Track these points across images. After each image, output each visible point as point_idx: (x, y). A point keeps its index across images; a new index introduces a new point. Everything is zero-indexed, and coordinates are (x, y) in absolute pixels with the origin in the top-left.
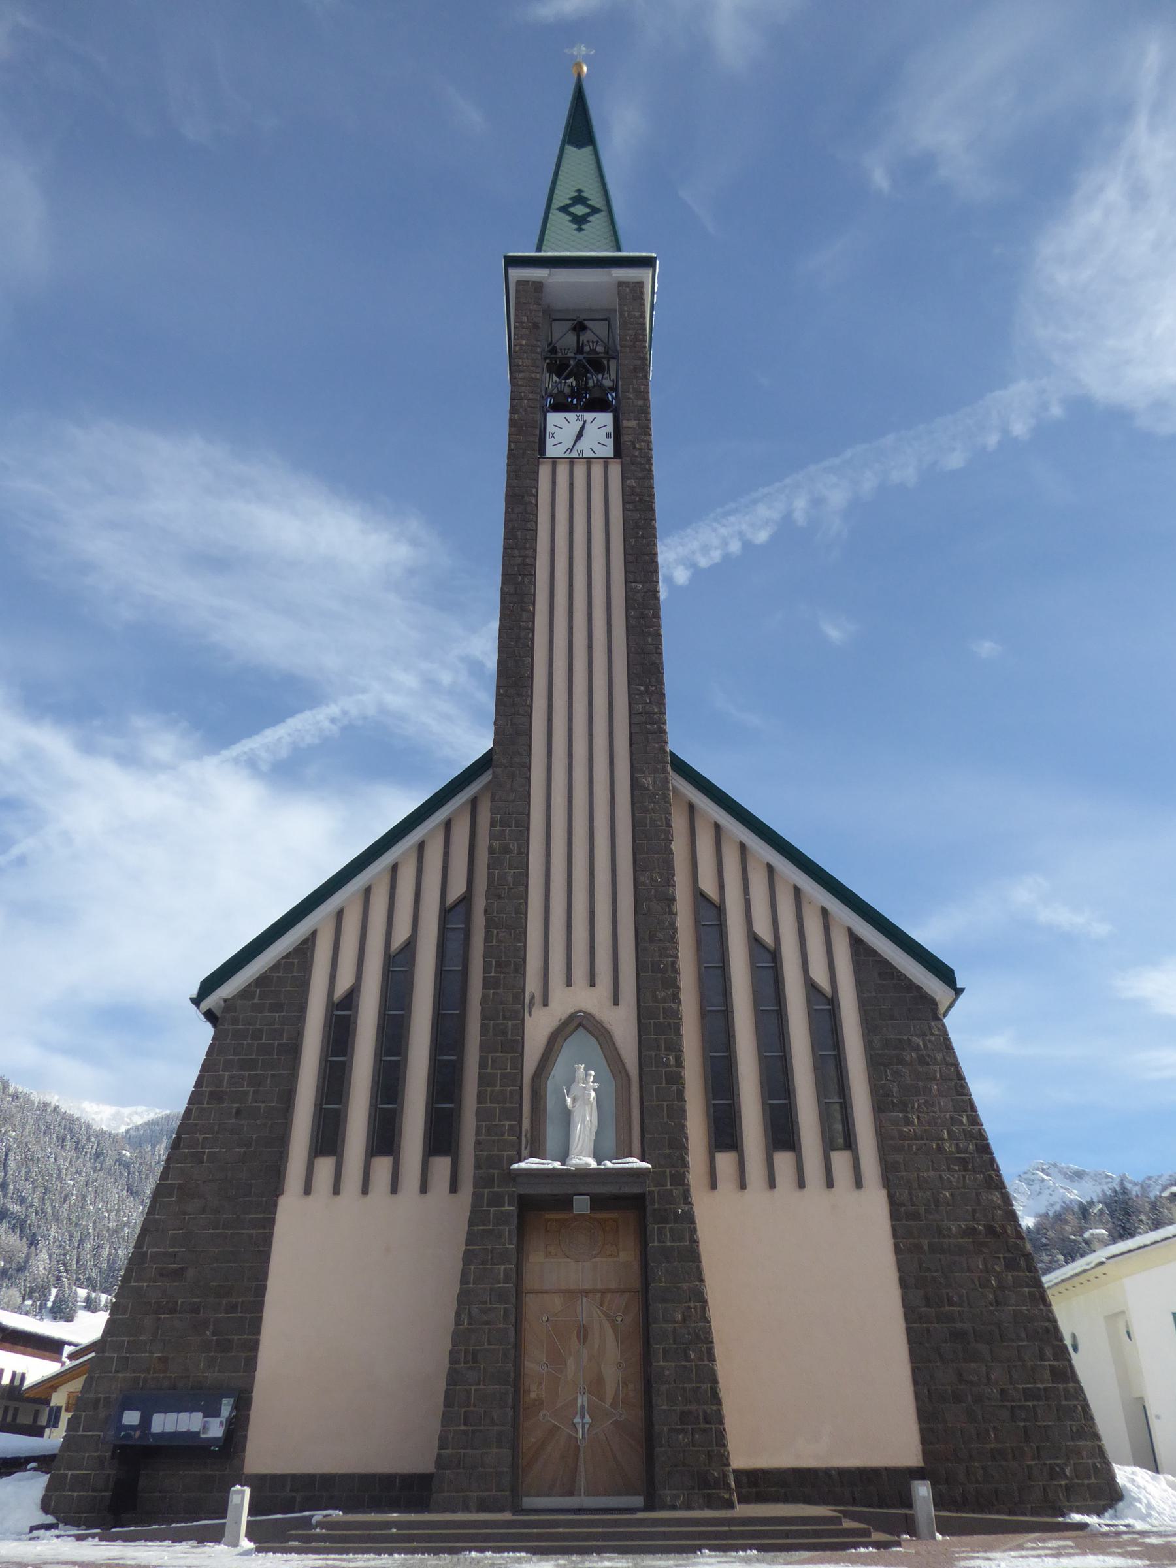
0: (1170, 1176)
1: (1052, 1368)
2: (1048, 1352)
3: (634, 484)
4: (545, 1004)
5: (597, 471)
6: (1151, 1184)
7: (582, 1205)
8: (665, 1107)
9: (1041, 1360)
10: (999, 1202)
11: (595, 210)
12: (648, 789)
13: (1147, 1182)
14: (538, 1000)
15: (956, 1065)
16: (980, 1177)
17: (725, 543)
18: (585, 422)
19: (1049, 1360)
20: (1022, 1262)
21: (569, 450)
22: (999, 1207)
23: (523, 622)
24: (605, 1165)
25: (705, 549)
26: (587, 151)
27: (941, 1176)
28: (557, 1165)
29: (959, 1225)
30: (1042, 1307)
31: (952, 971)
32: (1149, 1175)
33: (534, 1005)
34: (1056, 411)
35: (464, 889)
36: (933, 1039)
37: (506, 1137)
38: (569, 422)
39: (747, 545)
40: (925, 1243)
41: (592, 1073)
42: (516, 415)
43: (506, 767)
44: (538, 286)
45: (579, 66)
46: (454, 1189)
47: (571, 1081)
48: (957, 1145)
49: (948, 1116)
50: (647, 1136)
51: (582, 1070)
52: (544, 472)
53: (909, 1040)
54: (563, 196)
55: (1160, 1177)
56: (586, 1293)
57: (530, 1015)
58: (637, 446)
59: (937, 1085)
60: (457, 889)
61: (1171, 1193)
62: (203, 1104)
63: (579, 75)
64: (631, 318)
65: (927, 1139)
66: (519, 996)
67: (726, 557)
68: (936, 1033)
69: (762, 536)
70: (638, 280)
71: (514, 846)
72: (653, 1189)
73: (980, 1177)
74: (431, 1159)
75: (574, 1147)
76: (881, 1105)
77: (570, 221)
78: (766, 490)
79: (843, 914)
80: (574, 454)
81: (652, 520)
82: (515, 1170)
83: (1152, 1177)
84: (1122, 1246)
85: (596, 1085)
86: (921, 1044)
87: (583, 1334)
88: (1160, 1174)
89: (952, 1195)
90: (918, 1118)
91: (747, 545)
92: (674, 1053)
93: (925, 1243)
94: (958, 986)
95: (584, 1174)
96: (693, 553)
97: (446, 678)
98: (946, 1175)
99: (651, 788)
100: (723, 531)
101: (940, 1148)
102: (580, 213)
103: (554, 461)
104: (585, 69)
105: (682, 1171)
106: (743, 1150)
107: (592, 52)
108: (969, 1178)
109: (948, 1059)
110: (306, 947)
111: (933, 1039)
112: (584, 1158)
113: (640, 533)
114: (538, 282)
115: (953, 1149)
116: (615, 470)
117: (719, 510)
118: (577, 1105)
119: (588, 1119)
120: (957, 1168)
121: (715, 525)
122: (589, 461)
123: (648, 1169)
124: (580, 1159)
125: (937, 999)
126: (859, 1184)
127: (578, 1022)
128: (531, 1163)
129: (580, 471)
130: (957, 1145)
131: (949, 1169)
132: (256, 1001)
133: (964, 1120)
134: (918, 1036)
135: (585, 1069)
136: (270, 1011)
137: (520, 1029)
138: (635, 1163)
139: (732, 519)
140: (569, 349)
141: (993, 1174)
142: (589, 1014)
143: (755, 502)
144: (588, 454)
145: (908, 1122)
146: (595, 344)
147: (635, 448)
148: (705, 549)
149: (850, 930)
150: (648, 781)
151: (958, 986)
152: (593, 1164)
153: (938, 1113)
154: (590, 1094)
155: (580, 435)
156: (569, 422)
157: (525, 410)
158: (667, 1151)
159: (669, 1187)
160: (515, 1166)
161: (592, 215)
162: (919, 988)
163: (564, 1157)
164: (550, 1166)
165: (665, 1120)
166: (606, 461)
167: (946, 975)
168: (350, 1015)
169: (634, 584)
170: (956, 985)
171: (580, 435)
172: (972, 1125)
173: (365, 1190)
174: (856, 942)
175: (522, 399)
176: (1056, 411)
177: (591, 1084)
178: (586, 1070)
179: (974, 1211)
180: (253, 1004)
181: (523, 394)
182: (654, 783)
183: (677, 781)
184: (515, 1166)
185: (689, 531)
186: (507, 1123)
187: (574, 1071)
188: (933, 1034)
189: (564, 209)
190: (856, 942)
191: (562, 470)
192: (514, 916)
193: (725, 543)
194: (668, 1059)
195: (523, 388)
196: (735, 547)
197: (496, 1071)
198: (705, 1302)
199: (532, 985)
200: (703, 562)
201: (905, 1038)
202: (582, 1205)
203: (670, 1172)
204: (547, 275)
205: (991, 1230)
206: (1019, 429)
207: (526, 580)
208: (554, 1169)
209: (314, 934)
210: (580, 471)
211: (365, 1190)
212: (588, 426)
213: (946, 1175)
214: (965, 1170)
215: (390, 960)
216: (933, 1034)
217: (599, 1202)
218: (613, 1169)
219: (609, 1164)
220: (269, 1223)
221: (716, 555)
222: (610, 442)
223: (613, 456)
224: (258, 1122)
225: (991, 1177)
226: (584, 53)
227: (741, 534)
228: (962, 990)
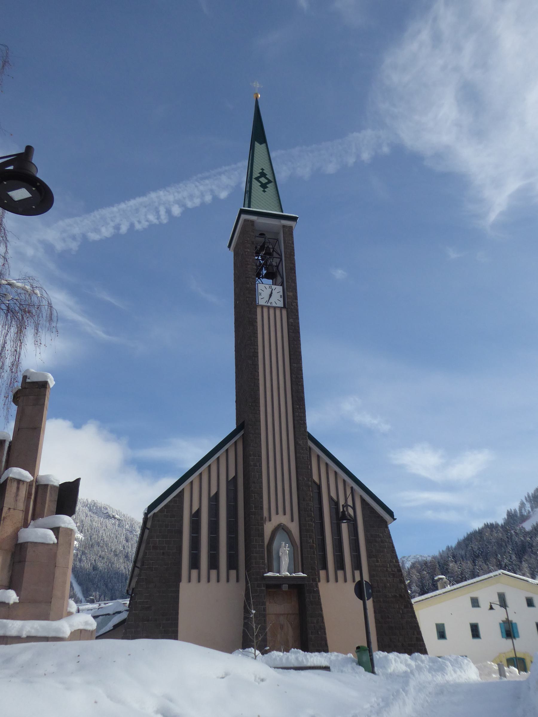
0: (414, 556)
1: (417, 638)
2: (416, 633)
3: (293, 322)
4: (270, 520)
5: (278, 312)
6: (404, 560)
7: (285, 587)
8: (310, 556)
9: (414, 635)
10: (404, 587)
11: (269, 182)
12: (301, 446)
13: (402, 559)
14: (267, 519)
15: (392, 543)
16: (398, 579)
17: (202, 195)
18: (272, 289)
19: (416, 635)
20: (409, 606)
21: (268, 301)
22: (403, 589)
23: (256, 376)
24: (293, 575)
25: (191, 197)
26: (264, 145)
27: (387, 579)
28: (278, 575)
29: (391, 594)
30: (414, 619)
31: (393, 512)
32: (404, 556)
33: (266, 521)
34: (386, 149)
35: (234, 475)
36: (386, 534)
37: (261, 565)
38: (278, 300)
39: (215, 199)
40: (382, 600)
41: (288, 545)
42: (248, 285)
43: (253, 434)
44: (252, 222)
45: (257, 94)
46: (238, 580)
47: (280, 546)
48: (392, 569)
49: (389, 560)
50: (304, 566)
51: (284, 544)
52: (259, 310)
53: (379, 535)
54: (256, 174)
55: (409, 557)
56: (283, 614)
57: (265, 524)
58: (293, 304)
59: (386, 549)
60: (232, 475)
61: (438, 578)
62: (150, 550)
63: (257, 99)
64: (289, 244)
65: (383, 567)
66: (262, 518)
67: (203, 204)
68: (387, 532)
69: (223, 195)
70: (291, 226)
71: (258, 464)
72: (307, 582)
73: (398, 579)
74: (230, 571)
75: (282, 569)
76: (369, 556)
77: (260, 186)
78: (227, 168)
79: (356, 487)
80: (269, 304)
81: (471, 534)
82: (266, 576)
83: (406, 557)
84: (423, 597)
85: (289, 549)
86: (382, 536)
87: (282, 627)
88: (409, 555)
89: (390, 585)
90: (381, 560)
91: (215, 199)
92: (312, 539)
93: (382, 600)
94: (395, 518)
95: (286, 578)
96: (184, 198)
97: (30, 252)
98: (388, 579)
99: (302, 445)
100: (201, 188)
101: (387, 570)
102: (264, 182)
103: (262, 307)
104: (259, 96)
105: (315, 577)
106: (328, 569)
107: (262, 87)
108: (395, 580)
109: (390, 541)
110: (181, 495)
111: (386, 534)
112: (286, 573)
113: (295, 343)
114: (253, 221)
115: (391, 570)
116: (284, 312)
117: (200, 175)
118: (283, 555)
119: (286, 560)
120: (392, 576)
121: (197, 184)
122: (275, 308)
123: (306, 576)
124: (285, 573)
125: (387, 521)
126: (345, 581)
127: (280, 527)
128: (270, 574)
129: (272, 311)
130: (392, 569)
131: (389, 577)
132: (165, 513)
133: (394, 561)
134: (381, 533)
135: (285, 543)
136: (171, 518)
137: (263, 529)
138: (301, 574)
139: (207, 182)
140: (258, 244)
141: (402, 579)
142: (285, 525)
143: (220, 174)
144: (274, 305)
145: (377, 561)
146: (269, 244)
147: (292, 305)
148: (191, 197)
149: (361, 496)
150: (301, 442)
151: (395, 518)
152: (289, 575)
153: (387, 559)
154: (287, 552)
155: (271, 296)
156: (278, 300)
157: (251, 283)
158: (310, 571)
159: (311, 582)
160: (266, 575)
161: (268, 184)
162: (382, 517)
163: (279, 572)
164: (276, 575)
165: (310, 561)
166: (281, 308)
167: (391, 513)
168: (193, 518)
169: (293, 364)
170: (394, 517)
171: (271, 296)
172: (396, 563)
173: (209, 581)
174: (363, 501)
175: (249, 278)
176: (386, 149)
177: (287, 548)
178: (285, 544)
179: (396, 590)
180: (164, 514)
181: (250, 276)
182: (303, 443)
183: (310, 444)
184: (266, 575)
185: (181, 185)
186: (261, 561)
187: (281, 544)
188: (386, 533)
189: (257, 179)
190: (363, 501)
191: (265, 310)
192: (259, 489)
193: (202, 195)
194: (310, 541)
195: (250, 272)
196: (208, 198)
197: (256, 543)
198: (323, 617)
199: (266, 514)
200: (189, 204)
201: (377, 534)
202: (285, 587)
203: (312, 577)
204: (256, 219)
205: (401, 596)
206: (366, 156)
207: (256, 359)
208: (278, 576)
209: (183, 489)
210: (272, 311)
211: (209, 581)
212: (273, 291)
213: (388, 579)
214: (394, 577)
215: (210, 499)
216: (386, 533)
217: (290, 586)
218: (295, 576)
219: (294, 575)
220: (177, 592)
221: (197, 201)
222: (282, 299)
223: (283, 306)
224: (171, 557)
225: (401, 579)
226: (258, 86)
227: (212, 191)
228: (396, 519)
